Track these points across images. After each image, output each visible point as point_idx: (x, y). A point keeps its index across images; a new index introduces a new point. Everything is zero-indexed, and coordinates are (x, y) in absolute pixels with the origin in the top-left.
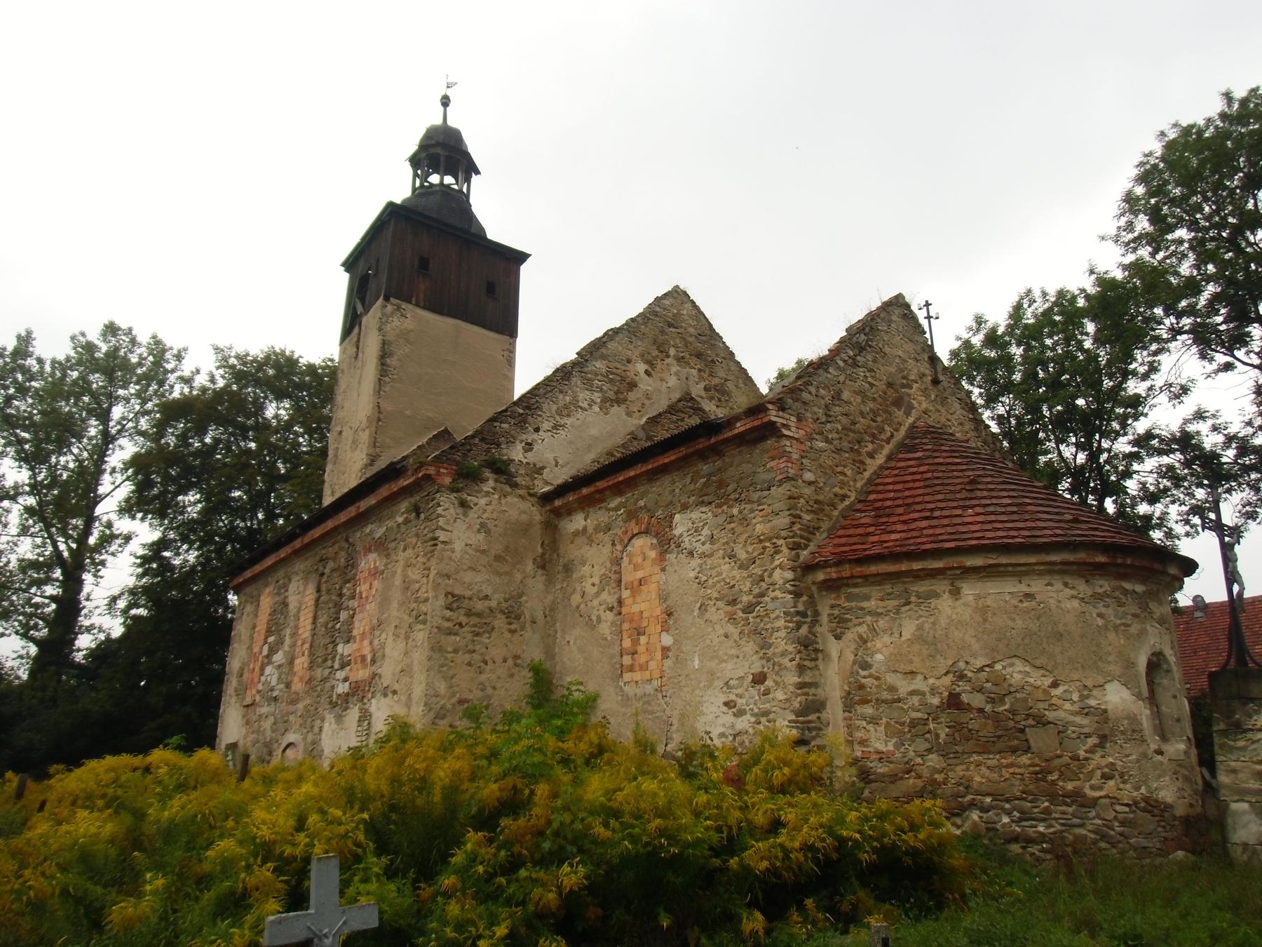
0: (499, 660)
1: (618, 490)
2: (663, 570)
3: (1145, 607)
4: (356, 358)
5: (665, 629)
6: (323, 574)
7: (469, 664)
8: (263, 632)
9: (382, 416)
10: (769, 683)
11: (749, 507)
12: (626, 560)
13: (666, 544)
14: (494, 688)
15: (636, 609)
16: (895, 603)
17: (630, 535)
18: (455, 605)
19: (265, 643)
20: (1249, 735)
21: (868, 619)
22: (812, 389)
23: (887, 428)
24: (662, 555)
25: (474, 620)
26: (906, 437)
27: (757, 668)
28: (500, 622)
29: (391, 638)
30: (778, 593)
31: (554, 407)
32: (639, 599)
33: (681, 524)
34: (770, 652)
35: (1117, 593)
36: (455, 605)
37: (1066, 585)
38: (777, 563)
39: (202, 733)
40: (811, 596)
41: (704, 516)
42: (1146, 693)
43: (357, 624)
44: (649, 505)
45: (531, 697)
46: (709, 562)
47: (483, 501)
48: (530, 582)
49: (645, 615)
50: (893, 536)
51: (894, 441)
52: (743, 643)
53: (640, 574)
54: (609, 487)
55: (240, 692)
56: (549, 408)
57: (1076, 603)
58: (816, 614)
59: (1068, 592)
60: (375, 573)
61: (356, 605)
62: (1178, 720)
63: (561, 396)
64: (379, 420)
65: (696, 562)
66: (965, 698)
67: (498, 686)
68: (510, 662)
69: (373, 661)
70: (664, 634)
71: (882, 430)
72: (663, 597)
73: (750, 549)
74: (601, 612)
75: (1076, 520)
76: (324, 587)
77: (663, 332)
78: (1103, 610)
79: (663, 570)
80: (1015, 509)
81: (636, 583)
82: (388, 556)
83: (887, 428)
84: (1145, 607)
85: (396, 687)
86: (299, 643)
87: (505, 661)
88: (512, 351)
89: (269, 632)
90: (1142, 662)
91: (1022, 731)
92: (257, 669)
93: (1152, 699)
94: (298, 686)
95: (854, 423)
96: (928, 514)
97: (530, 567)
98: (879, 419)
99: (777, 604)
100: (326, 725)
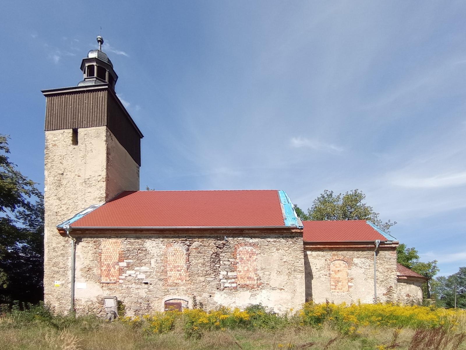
1: (331, 249)
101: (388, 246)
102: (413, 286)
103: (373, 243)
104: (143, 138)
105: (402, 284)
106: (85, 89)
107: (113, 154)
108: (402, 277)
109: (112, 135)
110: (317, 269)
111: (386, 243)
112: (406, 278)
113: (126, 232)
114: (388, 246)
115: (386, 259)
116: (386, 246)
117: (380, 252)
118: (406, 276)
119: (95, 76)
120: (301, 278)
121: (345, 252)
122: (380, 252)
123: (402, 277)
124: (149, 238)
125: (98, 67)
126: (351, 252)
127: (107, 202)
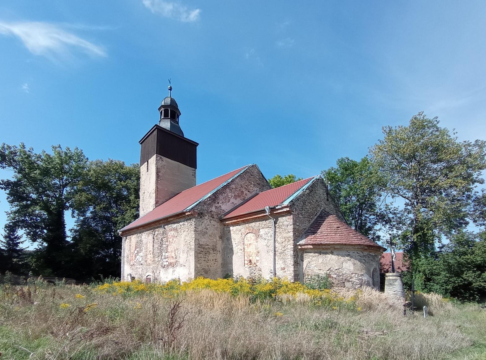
0: (212, 260)
1: (244, 222)
2: (257, 242)
3: (374, 259)
4: (148, 171)
5: (257, 255)
6: (154, 235)
7: (204, 261)
8: (134, 247)
9: (158, 190)
10: (286, 270)
11: (282, 230)
12: (245, 239)
13: (258, 236)
14: (211, 266)
15: (249, 250)
16: (318, 254)
17: (247, 233)
18: (200, 247)
19: (135, 250)
20: (393, 286)
21: (311, 257)
22: (299, 202)
23: (316, 212)
24: (257, 239)
25: (205, 250)
26: (320, 214)
27: (283, 266)
28: (212, 252)
29: (181, 253)
30: (289, 250)
31: (222, 197)
32: (249, 248)
33: (262, 232)
34: (286, 263)
35: (369, 255)
36: (200, 247)
37: (357, 253)
38: (289, 243)
39: (113, 270)
40: (297, 252)
41: (269, 231)
42: (372, 277)
43: (169, 249)
44: (252, 226)
45: (76, 231)
46: (270, 241)
47: (205, 221)
48: (218, 242)
49: (251, 252)
50: (318, 239)
51: (317, 215)
52: (279, 261)
53: (250, 242)
54: (241, 221)
55: (129, 262)
56: (221, 197)
57: (359, 257)
58: (298, 255)
59: (358, 255)
60: (174, 237)
61: (168, 244)
62: (378, 282)
63: (224, 194)
64: (158, 191)
65: (266, 241)
66: (332, 275)
67: (212, 266)
68: (214, 260)
69: (176, 258)
70: (257, 257)
71: (315, 213)
72: (257, 249)
73: (282, 239)
74: (238, 250)
75: (361, 239)
76: (155, 238)
77: (250, 177)
78: (365, 259)
79: (257, 242)
80: (347, 235)
81: (249, 244)
82: (178, 233)
83: (316, 212)
84: (374, 259)
85: (185, 264)
86: (148, 251)
87: (213, 260)
88: (194, 175)
89: (136, 248)
90: (372, 270)
91: (344, 283)
92: (134, 256)
93: (373, 278)
94: (149, 261)
95: (308, 211)
96: (326, 235)
97: (218, 238)
98: (314, 210)
99: (289, 253)
100: (161, 272)
101: (281, 211)
102: (329, 256)
103: (264, 211)
104: (199, 145)
105: (312, 254)
106: (147, 135)
107: (163, 171)
108: (306, 247)
109: (162, 157)
110: (236, 244)
111: (277, 208)
112: (311, 247)
113: (135, 230)
114: (281, 211)
115: (284, 226)
116: (279, 211)
117: (279, 218)
118: (312, 245)
119: (169, 117)
120: (272, 254)
121: (253, 224)
122: (279, 218)
123: (306, 247)
124: (283, 216)
125: (170, 110)
126: (258, 223)
127: (156, 207)
